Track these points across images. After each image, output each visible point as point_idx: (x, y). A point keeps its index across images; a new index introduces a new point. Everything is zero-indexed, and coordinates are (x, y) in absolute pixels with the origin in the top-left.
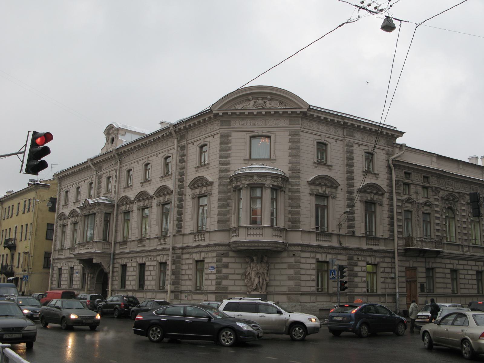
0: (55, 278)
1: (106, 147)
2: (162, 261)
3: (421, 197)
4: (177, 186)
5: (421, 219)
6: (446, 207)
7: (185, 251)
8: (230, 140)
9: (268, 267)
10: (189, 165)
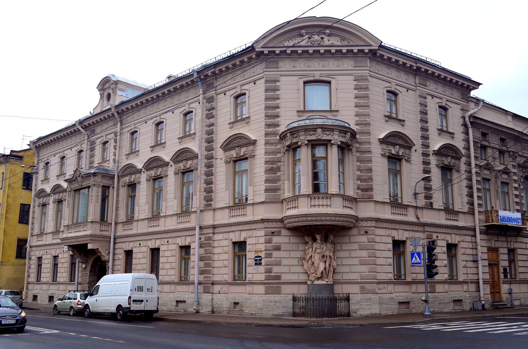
0: (33, 270)
1: (100, 105)
3: (498, 163)
4: (204, 148)
5: (500, 190)
6: (524, 176)
7: (217, 230)
8: (279, 86)
9: (334, 248)
10: (219, 120)
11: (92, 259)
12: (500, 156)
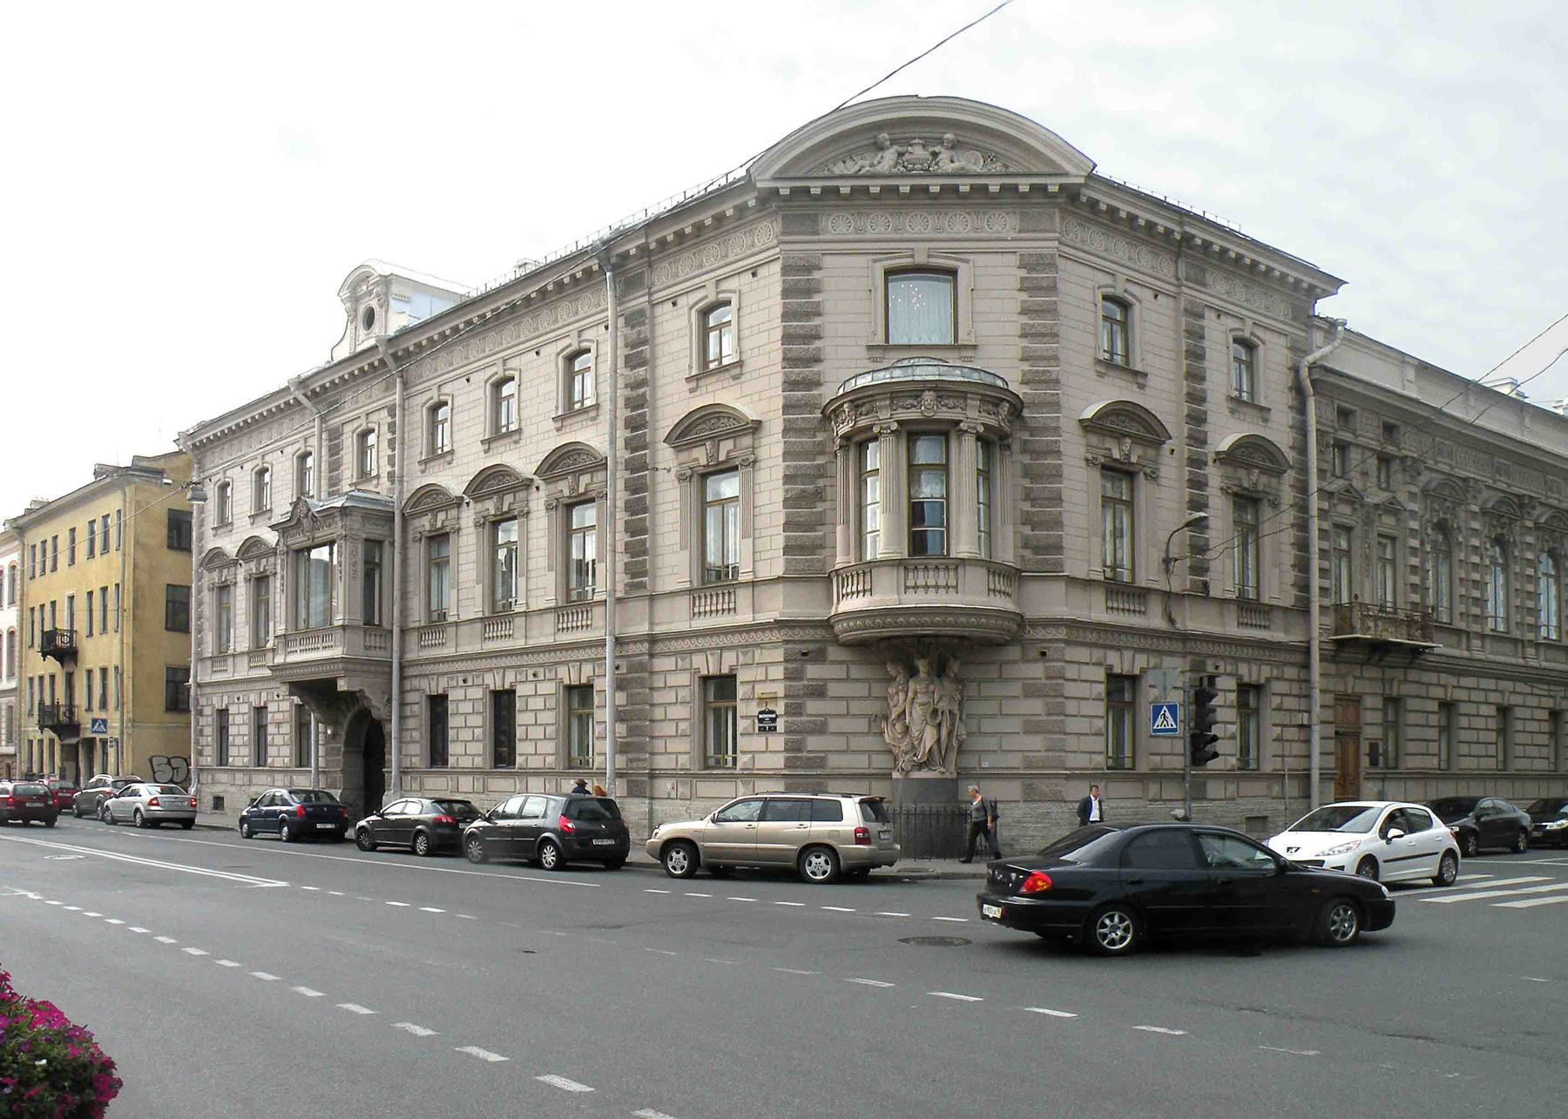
2: (575, 682)
4: (620, 443)
7: (659, 647)
9: (961, 693)
11: (349, 715)
12: (1379, 469)
